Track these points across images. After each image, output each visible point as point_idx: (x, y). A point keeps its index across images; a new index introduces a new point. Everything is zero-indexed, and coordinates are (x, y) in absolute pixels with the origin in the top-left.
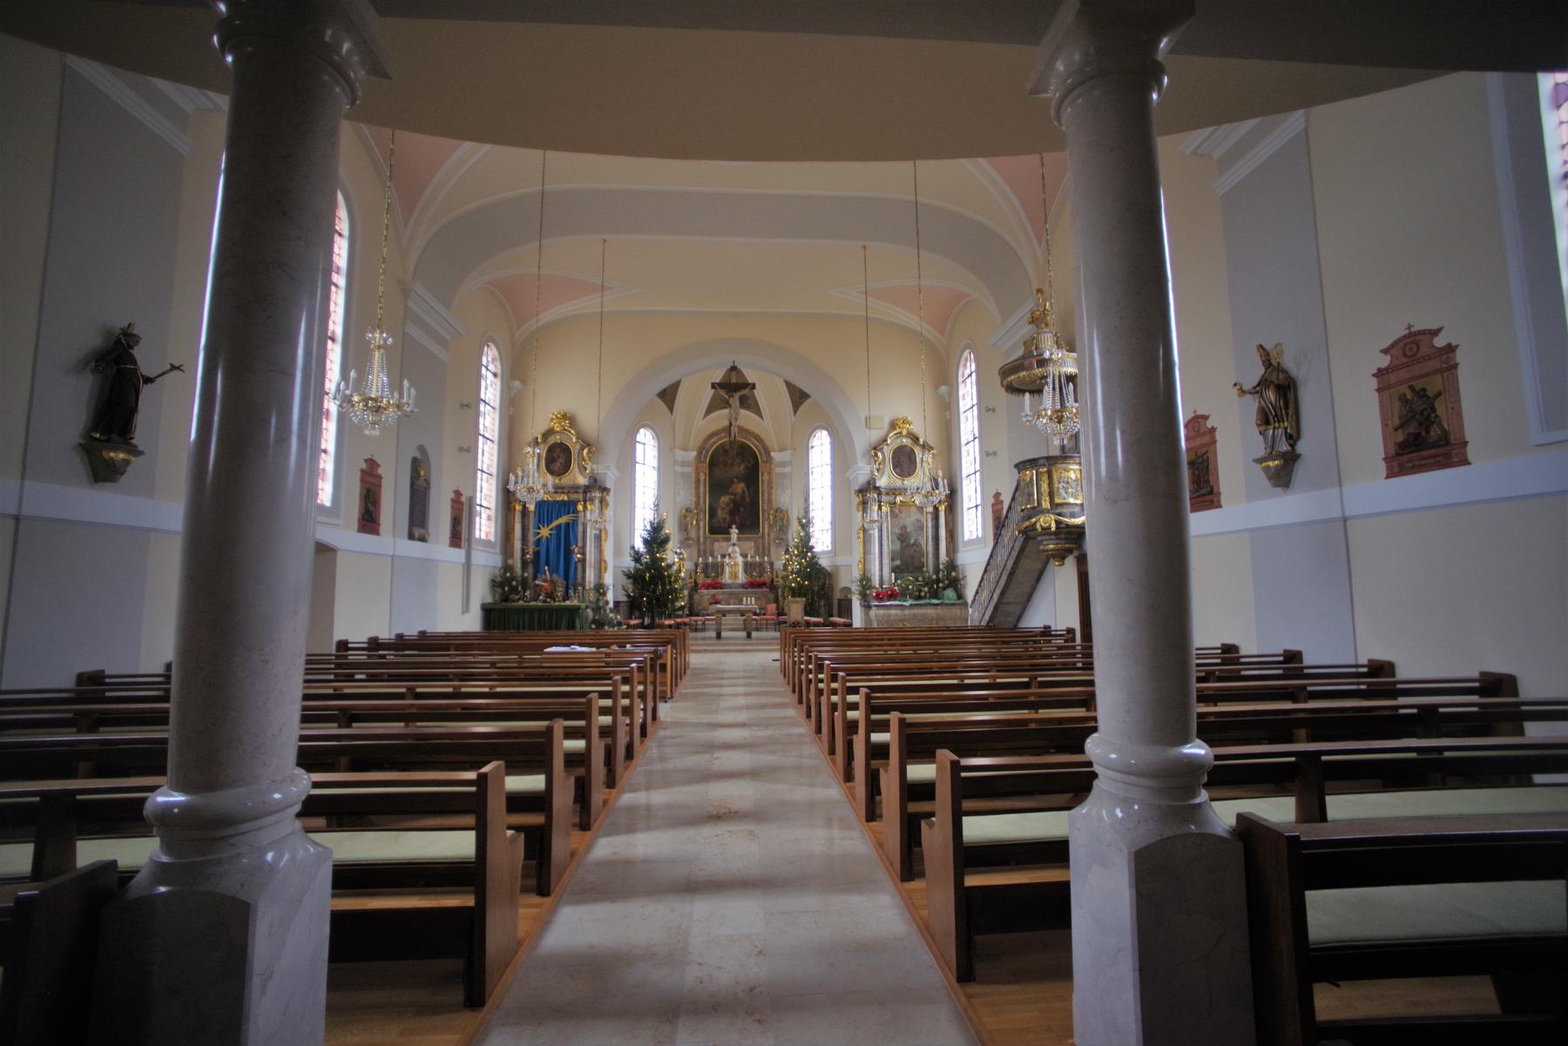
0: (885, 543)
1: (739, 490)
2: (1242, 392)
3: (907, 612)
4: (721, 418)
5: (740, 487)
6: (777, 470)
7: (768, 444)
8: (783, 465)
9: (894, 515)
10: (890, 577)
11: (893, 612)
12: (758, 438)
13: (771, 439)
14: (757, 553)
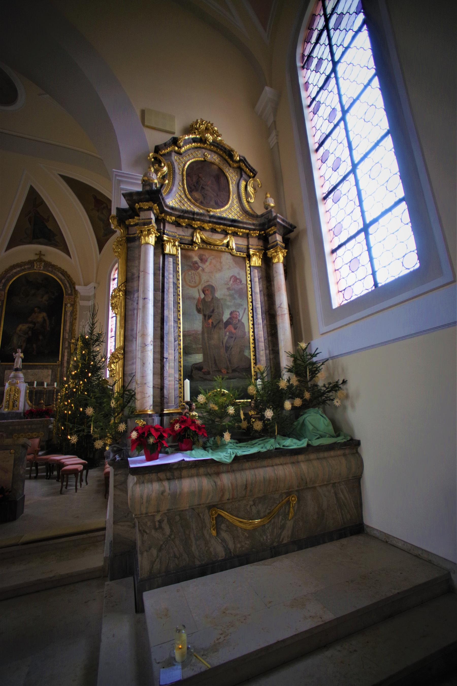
0: (170, 314)
1: (40, 319)
2: (61, 493)
3: (226, 479)
4: (27, 251)
5: (41, 316)
6: (82, 303)
7: (74, 280)
8: (87, 298)
9: (190, 266)
10: (180, 389)
11: (188, 484)
12: (64, 273)
13: (76, 274)
14: (53, 381)
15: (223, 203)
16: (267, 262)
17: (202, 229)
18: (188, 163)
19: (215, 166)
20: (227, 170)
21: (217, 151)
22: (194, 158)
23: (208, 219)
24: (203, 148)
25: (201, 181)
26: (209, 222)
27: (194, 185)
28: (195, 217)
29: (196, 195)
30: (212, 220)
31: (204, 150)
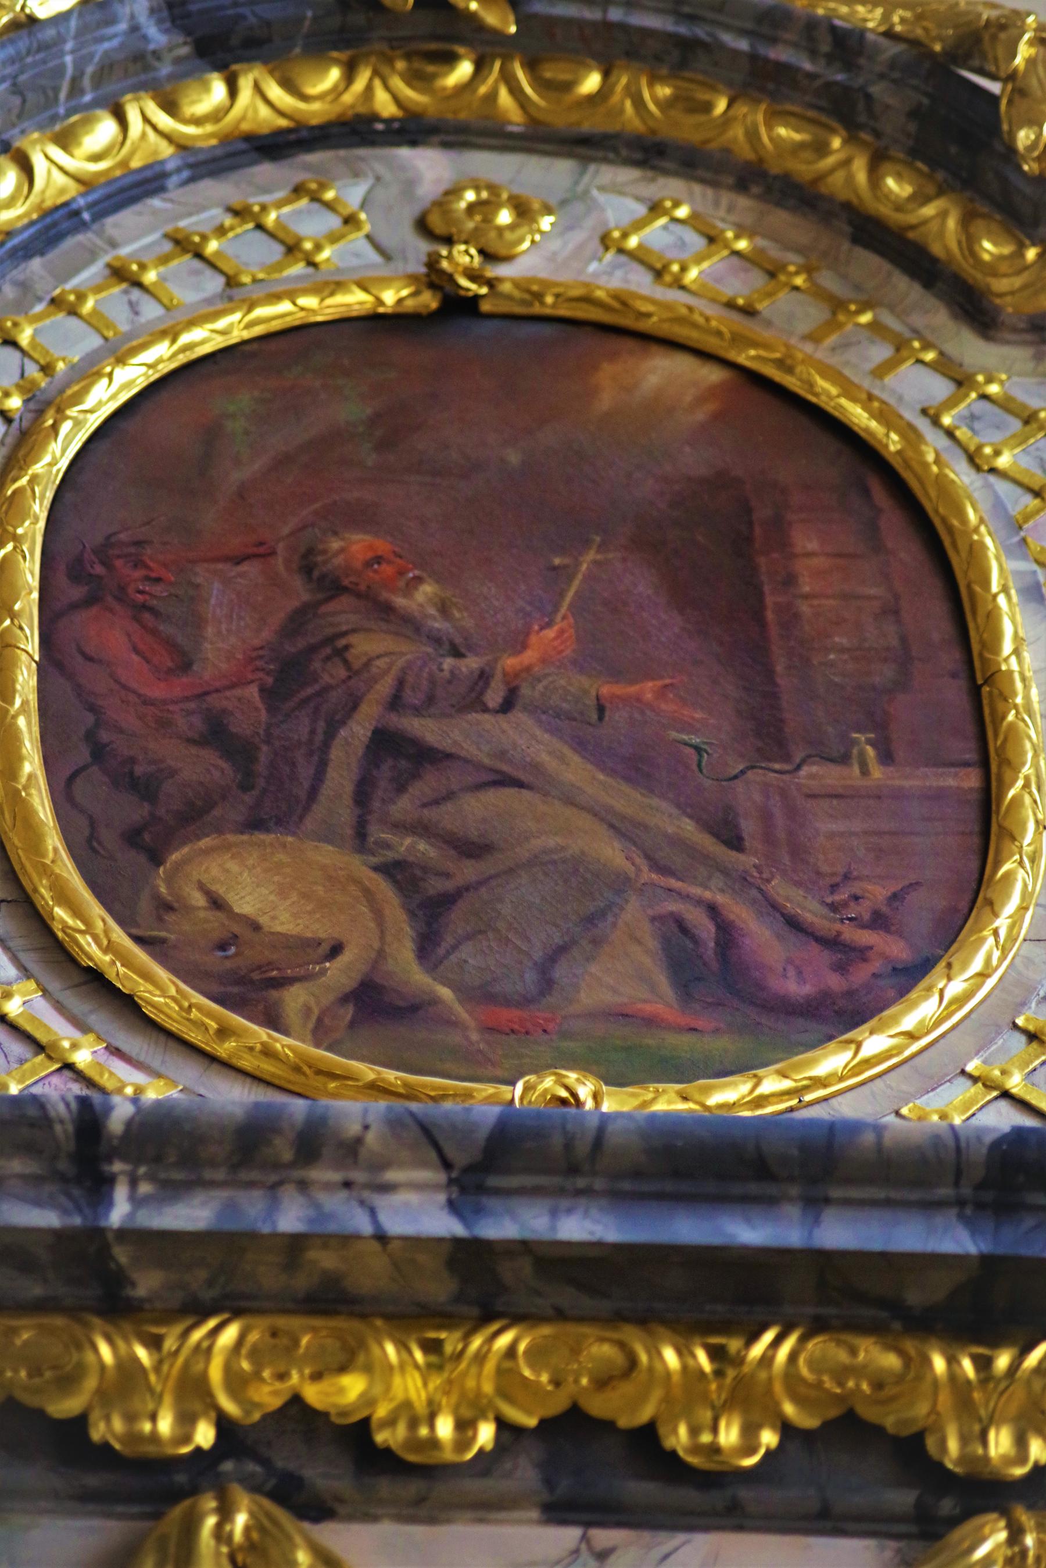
15: (845, 954)
16: (762, 768)
17: (324, 1474)
18: (103, 398)
19: (661, 372)
20: (916, 384)
21: (687, 130)
22: (234, 291)
23: (419, 1211)
24: (412, 130)
25: (365, 646)
26: (478, 1285)
27: (216, 733)
28: (120, 1211)
29: (252, 883)
30: (517, 1222)
31: (429, 167)
